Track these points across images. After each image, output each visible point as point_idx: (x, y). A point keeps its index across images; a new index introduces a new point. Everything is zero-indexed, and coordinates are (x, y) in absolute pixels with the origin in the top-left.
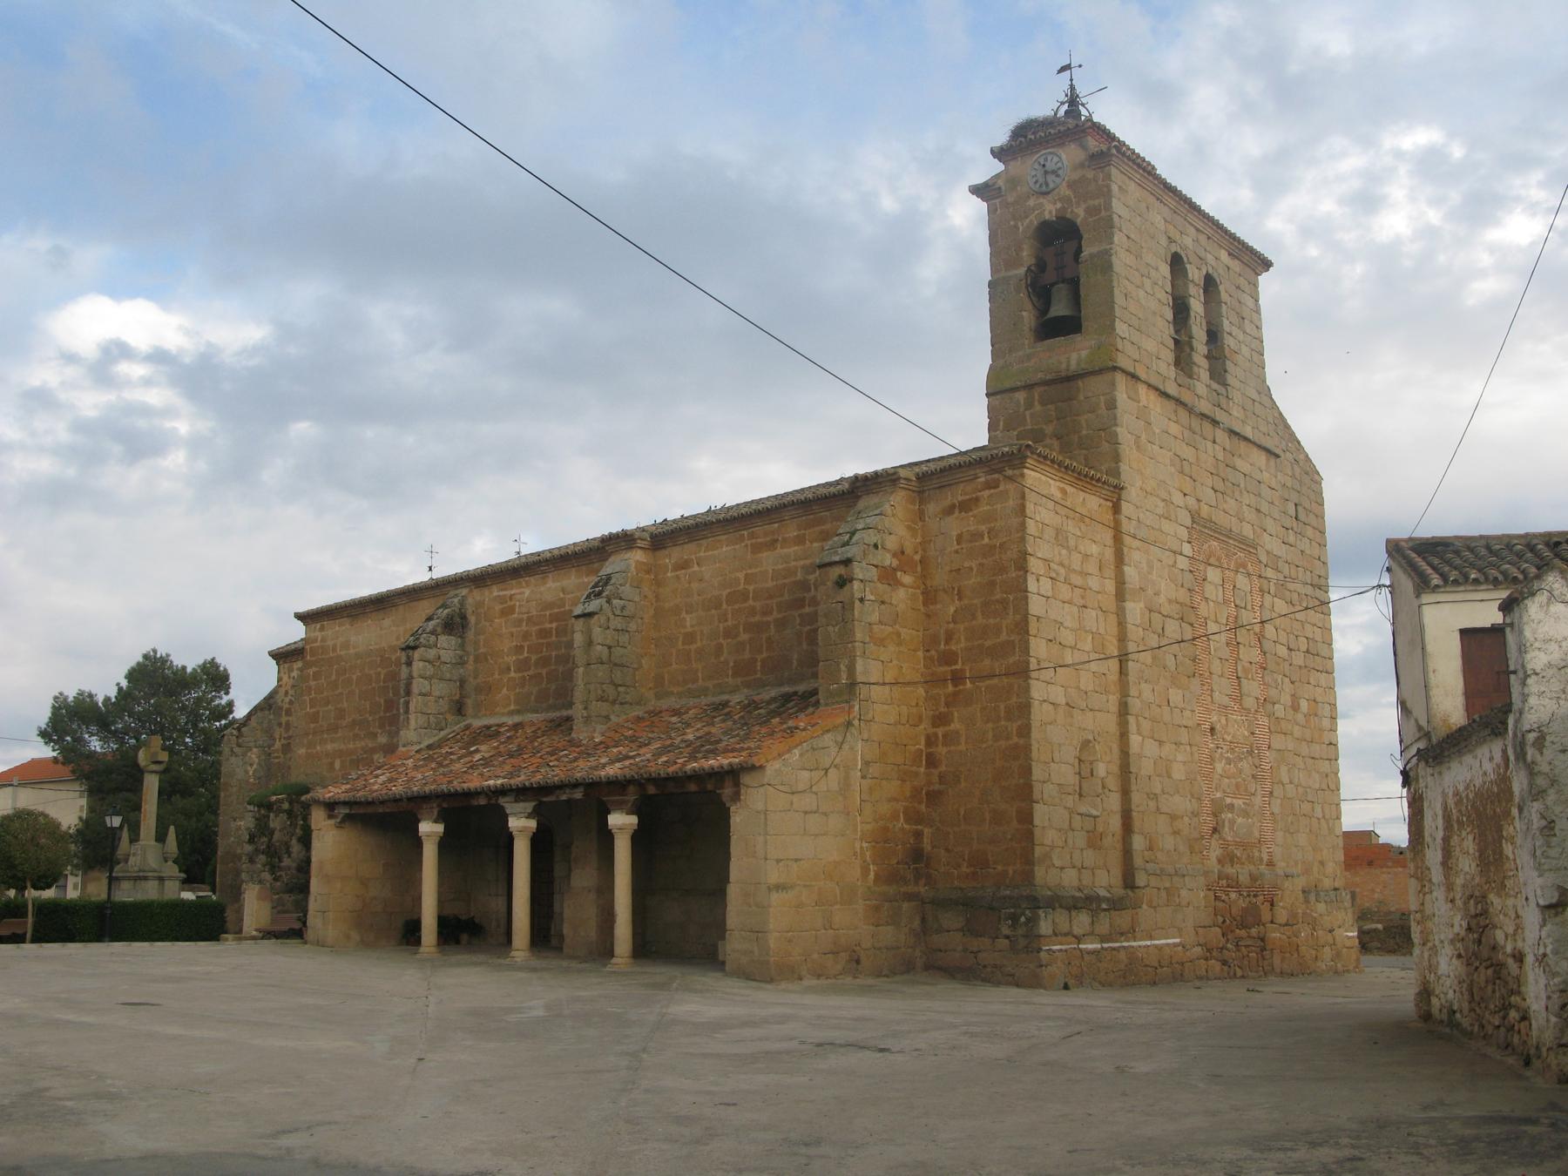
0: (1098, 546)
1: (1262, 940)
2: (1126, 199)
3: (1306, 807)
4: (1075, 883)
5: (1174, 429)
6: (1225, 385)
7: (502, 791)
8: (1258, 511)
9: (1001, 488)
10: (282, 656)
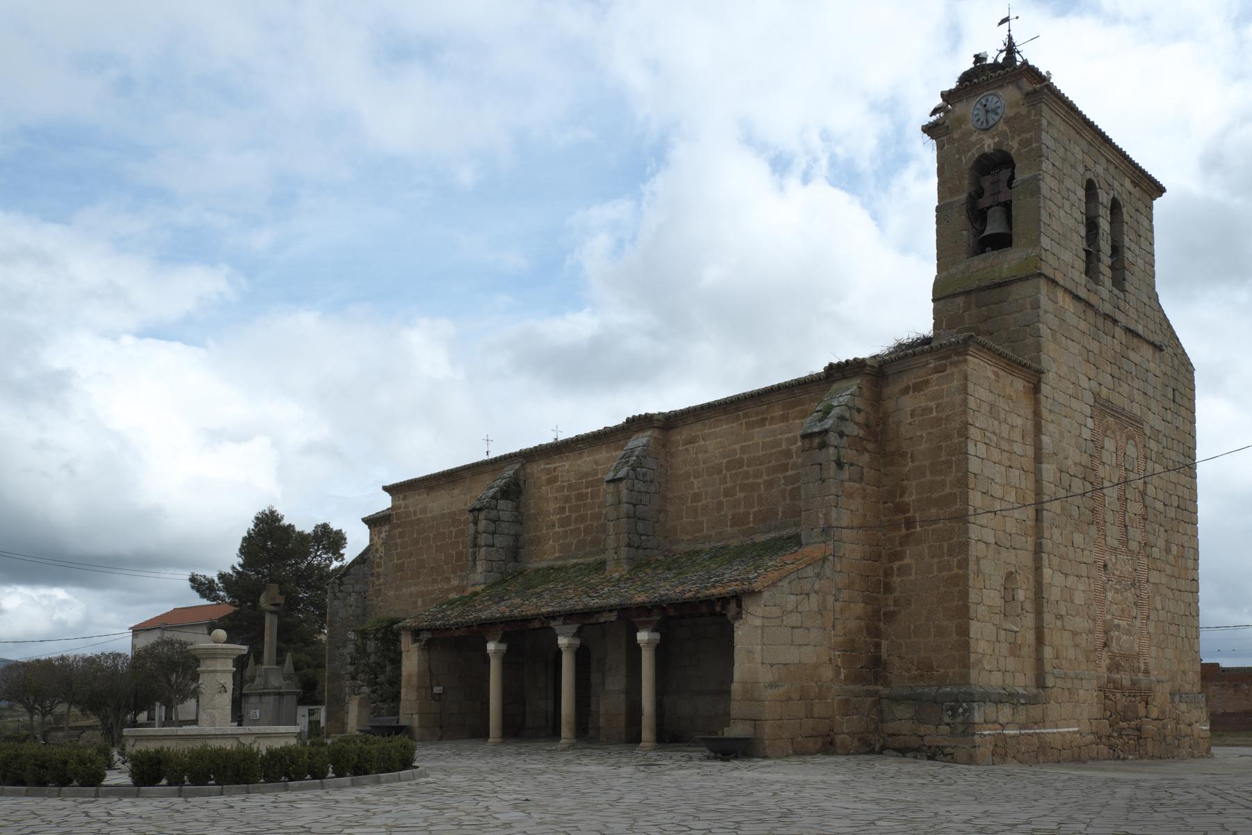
0: (1021, 420)
1: (1139, 730)
2: (1052, 135)
3: (1174, 629)
4: (1000, 684)
5: (1083, 326)
6: (1123, 291)
7: (552, 616)
8: (1145, 394)
9: (948, 371)
10: (371, 522)
